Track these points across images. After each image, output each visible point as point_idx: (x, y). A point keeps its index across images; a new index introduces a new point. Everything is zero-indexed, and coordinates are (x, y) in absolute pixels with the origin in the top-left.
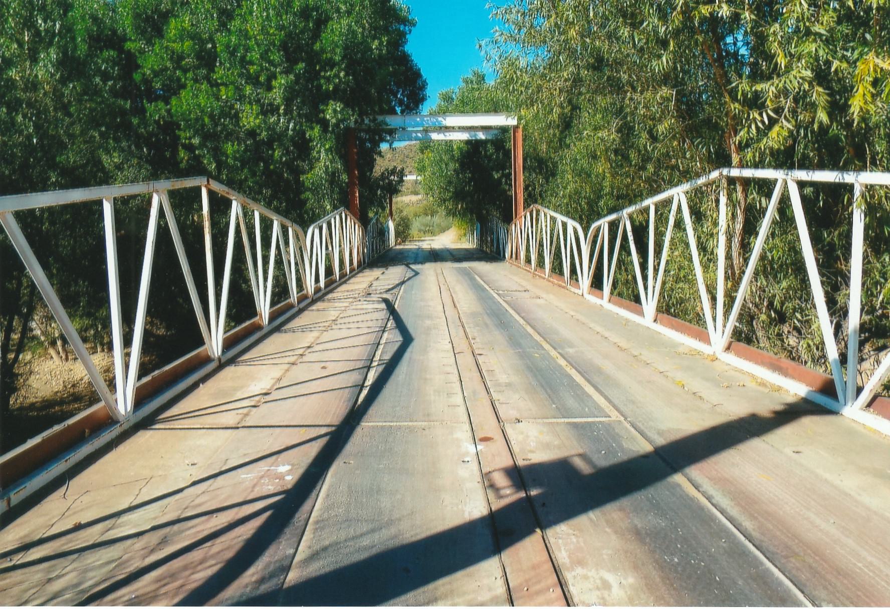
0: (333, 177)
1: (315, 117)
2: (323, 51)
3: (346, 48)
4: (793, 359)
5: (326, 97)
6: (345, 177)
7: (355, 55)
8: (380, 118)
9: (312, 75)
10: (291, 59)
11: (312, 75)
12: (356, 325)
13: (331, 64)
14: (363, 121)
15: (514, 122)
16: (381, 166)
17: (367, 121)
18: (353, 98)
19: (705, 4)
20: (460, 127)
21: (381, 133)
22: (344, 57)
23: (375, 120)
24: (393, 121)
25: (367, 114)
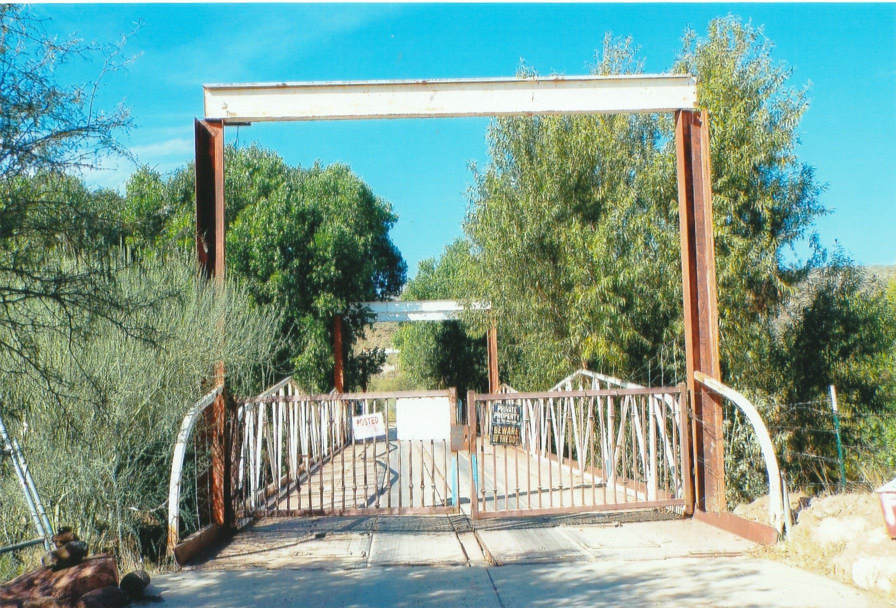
0: (320, 360)
1: (306, 306)
2: (315, 250)
3: (336, 245)
4: (828, 573)
5: (316, 289)
6: (331, 360)
7: (345, 254)
8: (364, 305)
9: (304, 270)
10: (287, 257)
11: (304, 270)
12: (360, 464)
13: (324, 260)
14: (348, 307)
15: (685, 96)
16: (359, 348)
17: (352, 308)
18: (344, 287)
19: (3, 447)
20: (437, 311)
21: (363, 319)
22: (334, 255)
23: (359, 306)
24: (376, 307)
25: (353, 301)
